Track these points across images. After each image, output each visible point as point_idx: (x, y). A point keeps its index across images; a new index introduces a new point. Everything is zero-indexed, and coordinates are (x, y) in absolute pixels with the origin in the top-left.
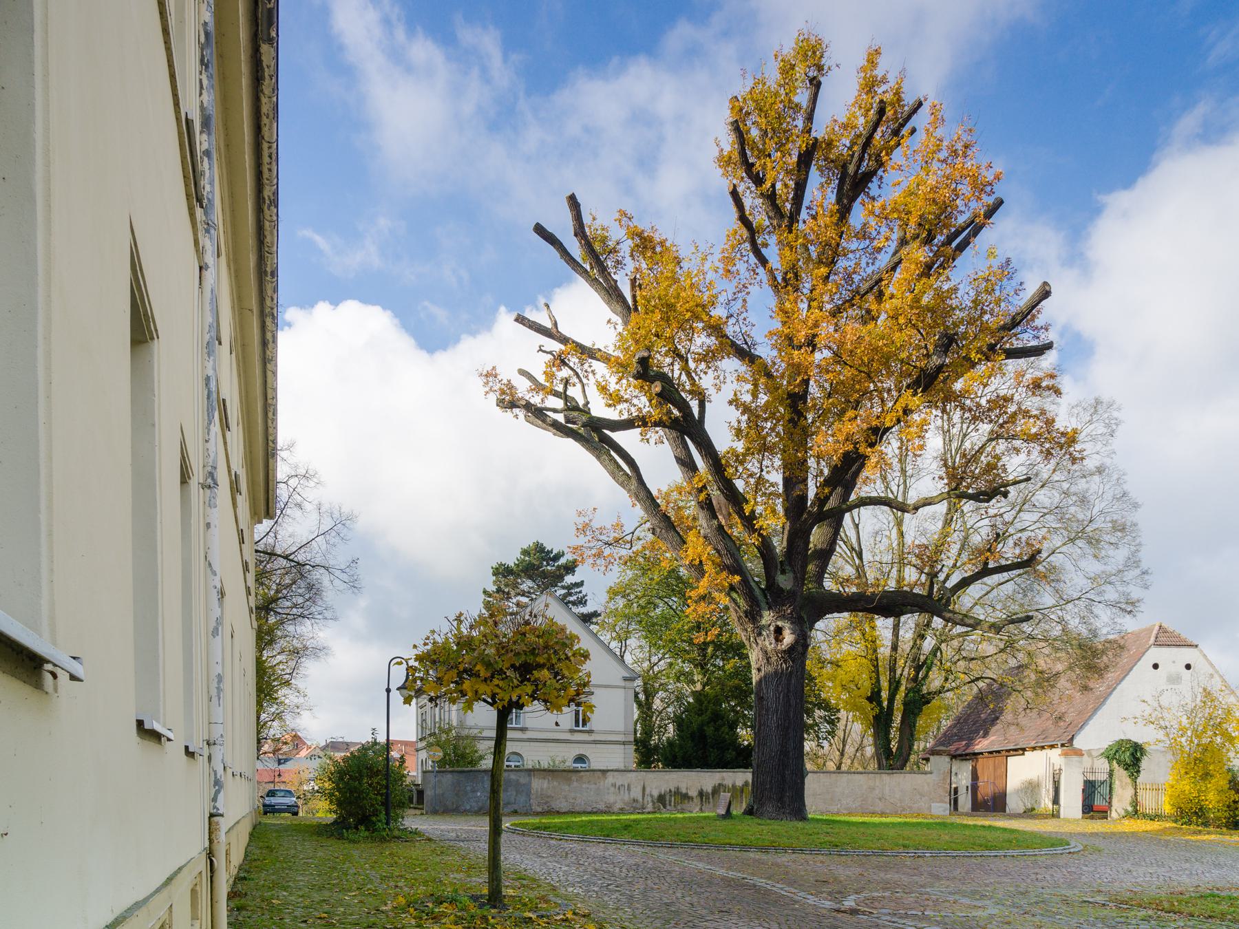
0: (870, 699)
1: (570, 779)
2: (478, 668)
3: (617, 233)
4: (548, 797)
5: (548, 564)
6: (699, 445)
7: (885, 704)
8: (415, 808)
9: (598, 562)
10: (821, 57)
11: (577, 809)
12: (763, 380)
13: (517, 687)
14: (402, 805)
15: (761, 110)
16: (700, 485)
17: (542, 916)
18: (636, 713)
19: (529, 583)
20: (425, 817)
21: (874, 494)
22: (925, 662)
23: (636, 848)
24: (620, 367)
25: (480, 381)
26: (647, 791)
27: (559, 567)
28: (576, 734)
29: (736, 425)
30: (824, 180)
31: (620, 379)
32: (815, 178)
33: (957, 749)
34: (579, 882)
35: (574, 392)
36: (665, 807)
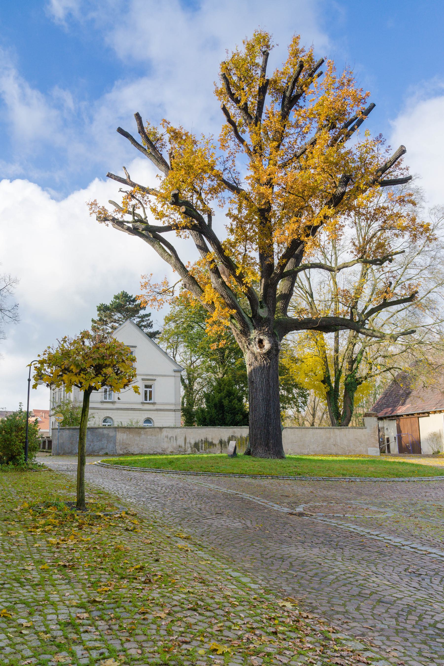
0: (324, 382)
1: (140, 433)
2: (71, 367)
3: (161, 131)
4: (127, 444)
5: (130, 304)
6: (209, 238)
7: (333, 385)
8: (47, 452)
9: (154, 303)
10: (268, 41)
11: (144, 452)
12: (245, 202)
13: (93, 378)
14: (34, 449)
15: (237, 68)
16: (211, 260)
17: (107, 515)
18: (183, 392)
19: (119, 315)
20: (51, 457)
21: (318, 261)
22: (355, 360)
23: (175, 476)
24: (164, 198)
25: (88, 208)
26: (188, 441)
27: (136, 306)
28: (145, 405)
29: (230, 226)
30: (274, 99)
31: (163, 205)
32: (268, 98)
33: (386, 413)
34: (135, 496)
35: (139, 211)
36: (199, 451)
